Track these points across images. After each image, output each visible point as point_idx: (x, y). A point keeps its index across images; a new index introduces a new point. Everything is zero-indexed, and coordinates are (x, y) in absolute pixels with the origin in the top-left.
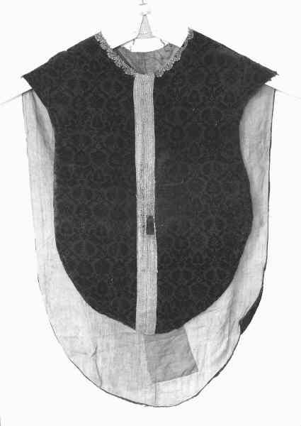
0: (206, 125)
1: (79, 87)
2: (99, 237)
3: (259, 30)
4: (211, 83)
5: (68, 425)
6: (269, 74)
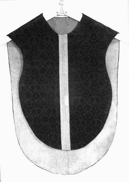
0: (91, 57)
1: (34, 39)
2: (27, 107)
3: (111, 14)
4: (92, 38)
5: (29, 181)
6: (116, 33)
